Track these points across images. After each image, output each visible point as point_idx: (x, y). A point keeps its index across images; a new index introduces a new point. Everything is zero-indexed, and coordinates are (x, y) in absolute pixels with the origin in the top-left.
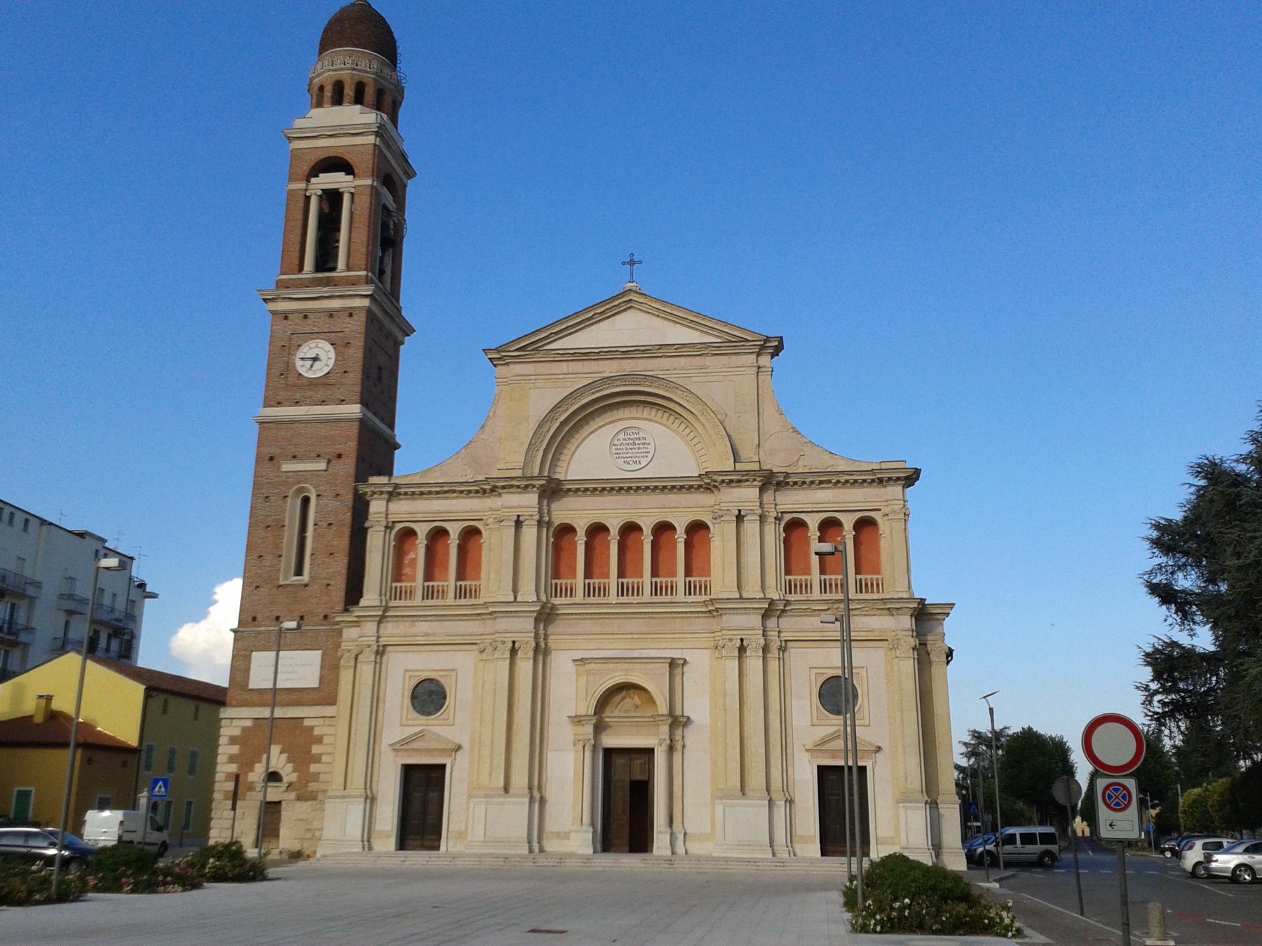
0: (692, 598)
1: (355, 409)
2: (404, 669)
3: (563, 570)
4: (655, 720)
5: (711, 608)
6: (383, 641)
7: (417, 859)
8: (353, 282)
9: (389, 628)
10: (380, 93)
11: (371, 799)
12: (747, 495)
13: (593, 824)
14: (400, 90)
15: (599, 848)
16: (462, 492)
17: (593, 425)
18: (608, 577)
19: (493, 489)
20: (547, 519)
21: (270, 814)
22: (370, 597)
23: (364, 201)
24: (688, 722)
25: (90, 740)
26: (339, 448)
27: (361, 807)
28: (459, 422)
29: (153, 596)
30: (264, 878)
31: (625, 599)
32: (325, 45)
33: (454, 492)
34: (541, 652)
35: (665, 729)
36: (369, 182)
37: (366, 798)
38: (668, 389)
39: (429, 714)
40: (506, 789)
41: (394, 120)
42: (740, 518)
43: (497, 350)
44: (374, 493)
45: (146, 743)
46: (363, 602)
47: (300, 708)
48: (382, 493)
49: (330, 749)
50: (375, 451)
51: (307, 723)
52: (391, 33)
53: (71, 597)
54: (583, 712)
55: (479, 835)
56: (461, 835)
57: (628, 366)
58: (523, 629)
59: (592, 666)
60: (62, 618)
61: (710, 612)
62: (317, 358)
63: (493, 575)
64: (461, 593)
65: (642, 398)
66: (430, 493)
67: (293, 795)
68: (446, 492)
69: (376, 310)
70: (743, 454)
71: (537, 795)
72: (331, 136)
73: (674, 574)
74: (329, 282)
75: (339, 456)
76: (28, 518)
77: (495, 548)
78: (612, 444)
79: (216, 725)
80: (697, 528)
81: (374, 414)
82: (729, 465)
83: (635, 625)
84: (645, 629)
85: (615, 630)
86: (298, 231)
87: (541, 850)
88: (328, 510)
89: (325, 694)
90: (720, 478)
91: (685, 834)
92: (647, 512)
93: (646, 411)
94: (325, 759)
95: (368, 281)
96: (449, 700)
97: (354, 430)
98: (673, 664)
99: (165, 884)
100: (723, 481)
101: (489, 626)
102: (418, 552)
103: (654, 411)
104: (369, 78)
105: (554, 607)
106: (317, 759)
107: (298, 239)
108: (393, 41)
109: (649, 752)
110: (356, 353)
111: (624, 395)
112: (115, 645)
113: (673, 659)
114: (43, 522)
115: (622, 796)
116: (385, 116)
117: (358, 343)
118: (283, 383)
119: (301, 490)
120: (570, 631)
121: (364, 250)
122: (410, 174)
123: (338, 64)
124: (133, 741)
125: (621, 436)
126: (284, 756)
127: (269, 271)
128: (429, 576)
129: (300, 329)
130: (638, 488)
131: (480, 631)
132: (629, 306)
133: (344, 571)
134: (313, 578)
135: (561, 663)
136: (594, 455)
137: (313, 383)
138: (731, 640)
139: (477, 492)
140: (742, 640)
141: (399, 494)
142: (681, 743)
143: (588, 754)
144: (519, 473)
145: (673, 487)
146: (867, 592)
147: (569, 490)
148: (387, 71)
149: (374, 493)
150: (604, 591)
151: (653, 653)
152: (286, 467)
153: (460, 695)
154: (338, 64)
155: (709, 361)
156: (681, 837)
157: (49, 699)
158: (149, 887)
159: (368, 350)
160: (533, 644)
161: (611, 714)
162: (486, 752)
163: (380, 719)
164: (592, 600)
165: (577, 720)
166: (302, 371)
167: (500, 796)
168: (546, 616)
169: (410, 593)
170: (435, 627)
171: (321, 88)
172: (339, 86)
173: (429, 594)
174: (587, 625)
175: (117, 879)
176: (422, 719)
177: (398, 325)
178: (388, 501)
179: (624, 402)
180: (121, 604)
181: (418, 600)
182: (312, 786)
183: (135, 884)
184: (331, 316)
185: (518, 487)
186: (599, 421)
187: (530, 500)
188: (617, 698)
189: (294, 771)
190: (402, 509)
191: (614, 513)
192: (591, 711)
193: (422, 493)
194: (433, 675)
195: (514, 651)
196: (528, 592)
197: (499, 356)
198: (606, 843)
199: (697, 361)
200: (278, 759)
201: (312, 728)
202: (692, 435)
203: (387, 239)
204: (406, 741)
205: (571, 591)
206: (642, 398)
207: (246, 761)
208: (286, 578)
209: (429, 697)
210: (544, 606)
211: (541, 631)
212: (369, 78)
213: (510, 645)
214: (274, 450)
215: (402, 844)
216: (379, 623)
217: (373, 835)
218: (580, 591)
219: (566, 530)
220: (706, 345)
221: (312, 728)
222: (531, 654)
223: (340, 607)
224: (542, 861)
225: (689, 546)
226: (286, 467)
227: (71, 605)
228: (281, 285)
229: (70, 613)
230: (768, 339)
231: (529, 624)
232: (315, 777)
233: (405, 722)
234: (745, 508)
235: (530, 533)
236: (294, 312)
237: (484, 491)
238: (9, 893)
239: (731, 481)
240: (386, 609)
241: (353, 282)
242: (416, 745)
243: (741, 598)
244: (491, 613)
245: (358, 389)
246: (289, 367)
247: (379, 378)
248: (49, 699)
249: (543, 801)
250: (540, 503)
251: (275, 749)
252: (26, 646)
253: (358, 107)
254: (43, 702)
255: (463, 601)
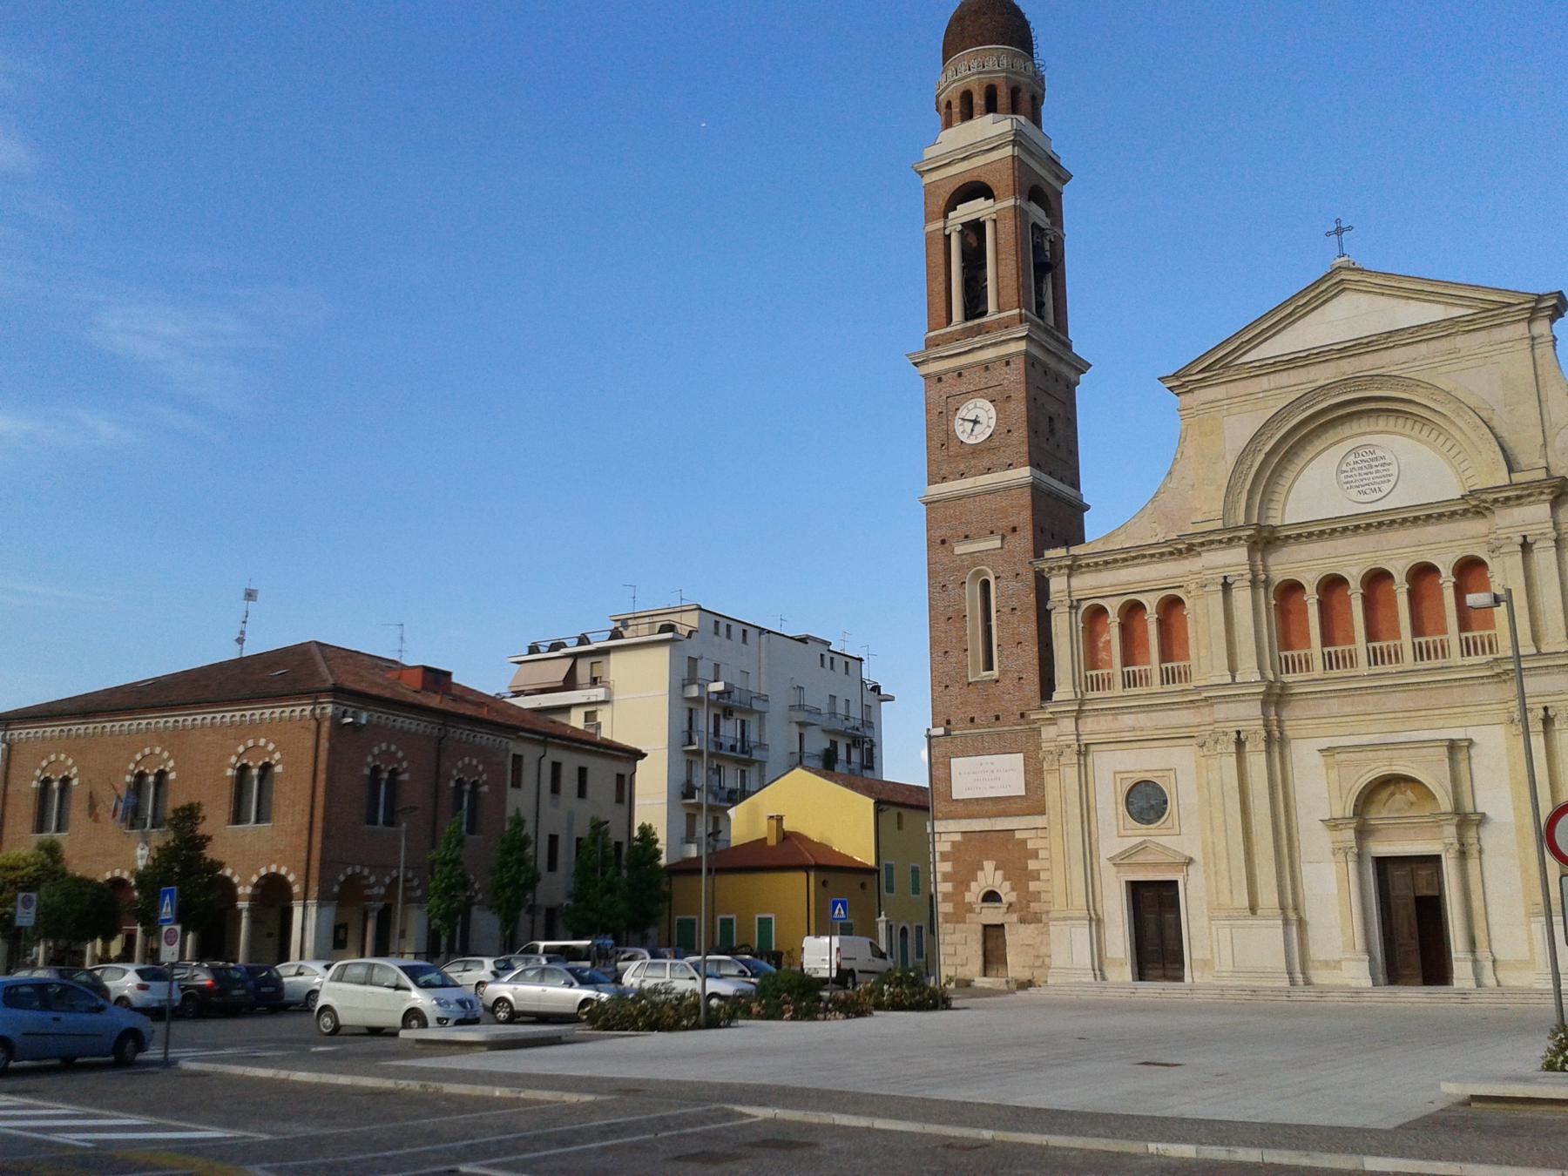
0: (1473, 659)
1: (1024, 473)
2: (1114, 769)
3: (1294, 639)
4: (1437, 821)
5: (1498, 670)
6: (1085, 739)
7: (1153, 990)
8: (1005, 325)
9: (1090, 725)
10: (1015, 92)
11: (1096, 921)
12: (1536, 515)
13: (1369, 950)
14: (1039, 81)
15: (1381, 978)
16: (1152, 556)
17: (1311, 451)
18: (1444, 632)
19: (1190, 548)
20: (1263, 577)
21: (993, 936)
22: (1063, 690)
23: (1008, 226)
24: (1482, 819)
25: (822, 862)
26: (1013, 521)
27: (1087, 930)
28: (1143, 467)
29: (890, 699)
30: (948, 1008)
31: (1380, 669)
32: (948, 51)
33: (1144, 556)
34: (1275, 741)
35: (1450, 831)
36: (1011, 202)
37: (1091, 920)
38: (1406, 388)
39: (1149, 822)
40: (1253, 909)
41: (1036, 121)
42: (1526, 547)
43: (1176, 376)
44: (1051, 569)
45: (883, 862)
46: (1056, 696)
47: (951, 822)
48: (1060, 568)
49: (1046, 864)
50: (1057, 519)
51: (1018, 835)
52: (1022, 16)
53: (801, 707)
54: (1338, 814)
55: (1227, 965)
56: (1207, 964)
57: (1347, 367)
58: (1248, 715)
59: (1343, 756)
60: (796, 730)
61: (1498, 675)
62: (978, 420)
63: (1203, 652)
64: (1168, 677)
65: (1373, 406)
66: (1116, 561)
67: (1014, 917)
68: (1134, 558)
69: (1036, 351)
70: (1523, 460)
71: (1292, 916)
72: (964, 159)
73: (1397, 635)
74: (979, 331)
75: (1014, 530)
76: (746, 629)
77: (1202, 616)
78: (1340, 471)
79: (924, 843)
80: (1470, 569)
81: (1050, 474)
82: (1502, 477)
83: (1397, 701)
84: (1411, 705)
85: (1370, 709)
86: (942, 278)
87: (1307, 982)
88: (1011, 593)
89: (1032, 802)
90: (1491, 497)
91: (1494, 961)
92: (1395, 555)
93: (1392, 421)
94: (1043, 875)
95: (1022, 319)
96: (1171, 806)
97: (1026, 498)
98: (1452, 746)
99: (826, 1010)
100: (1496, 500)
101: (1205, 715)
102: (1112, 633)
103: (1401, 421)
104: (999, 78)
105: (1284, 686)
106: (1035, 876)
107: (942, 287)
108: (1026, 24)
109: (1435, 860)
110: (1019, 408)
111: (1350, 405)
112: (855, 755)
113: (1452, 741)
114: (762, 630)
115: (1406, 919)
116: (1022, 119)
117: (1019, 394)
118: (947, 455)
119: (978, 573)
120: (1312, 713)
121: (1014, 284)
122: (1064, 177)
123: (963, 72)
124: (871, 862)
125: (1351, 458)
126: (999, 874)
127: (917, 330)
128: (1127, 660)
129: (956, 390)
130: (1381, 524)
131: (1196, 721)
132: (1340, 288)
133: (1036, 662)
134: (1003, 672)
135: (1305, 755)
136: (1317, 488)
137: (976, 450)
138: (1226, 734)
139: (1171, 553)
140: (1546, 709)
141: (1080, 566)
142: (1476, 847)
143: (1352, 866)
144: (1219, 525)
145: (1429, 516)
146: (1429, 658)
147: (1288, 537)
148: (1019, 63)
149: (1051, 569)
150: (1350, 660)
151: (1426, 735)
152: (960, 549)
153: (1184, 796)
154: (963, 72)
155: (1460, 341)
156: (1488, 965)
157: (780, 819)
158: (809, 1014)
159: (1033, 402)
160: (1263, 733)
161: (1377, 815)
162: (1223, 866)
163: (1093, 829)
164: (1335, 673)
165: (1333, 824)
166: (963, 438)
167: (1246, 918)
168: (1275, 698)
169: (1106, 683)
170: (1142, 719)
171: (949, 105)
172: (967, 97)
173: (1130, 681)
174: (1334, 705)
175: (780, 1006)
176: (1143, 829)
177: (1068, 363)
178: (1069, 576)
179: (1334, 420)
180: (855, 712)
181: (1118, 690)
182: (1034, 906)
183: (795, 1011)
184: (987, 368)
185: (1220, 541)
186: (1319, 444)
187: (1235, 558)
188: (1384, 794)
189: (1013, 889)
190: (1086, 584)
191: (1351, 560)
192: (1349, 812)
193: (1106, 563)
194: (1148, 776)
195: (1240, 743)
196: (1248, 670)
197: (1180, 382)
198: (1393, 972)
199: (1444, 344)
200: (989, 877)
201: (1025, 841)
202: (1448, 446)
203: (1044, 264)
204: (1128, 854)
205: (1307, 664)
206: (1373, 406)
207: (962, 880)
208: (976, 673)
209: (1147, 802)
210: (1270, 685)
211: (1273, 717)
212: (999, 78)
213: (1234, 736)
214: (944, 532)
215: (1141, 974)
216: (1077, 719)
217: (1106, 962)
218: (1318, 663)
219: (1292, 589)
220: (1453, 321)
221: (1025, 841)
222: (1262, 746)
223: (1037, 702)
224: (1300, 994)
225: (1414, 597)
226: (960, 549)
227: (802, 717)
228: (930, 343)
229: (801, 724)
230: (1540, 298)
231: (1255, 709)
232: (1036, 896)
233: (1123, 832)
234: (1532, 532)
235: (1242, 598)
236: (947, 372)
237: (1180, 552)
238: (658, 1019)
239: (1508, 499)
240: (1082, 702)
241: (1005, 325)
242: (1140, 858)
243: (1539, 653)
244: (1206, 699)
245: (1025, 448)
246: (949, 434)
247: (1052, 431)
248: (780, 819)
249: (1302, 923)
250: (1250, 558)
251: (989, 865)
252: (762, 763)
253: (991, 115)
254: (774, 822)
255: (1172, 687)
